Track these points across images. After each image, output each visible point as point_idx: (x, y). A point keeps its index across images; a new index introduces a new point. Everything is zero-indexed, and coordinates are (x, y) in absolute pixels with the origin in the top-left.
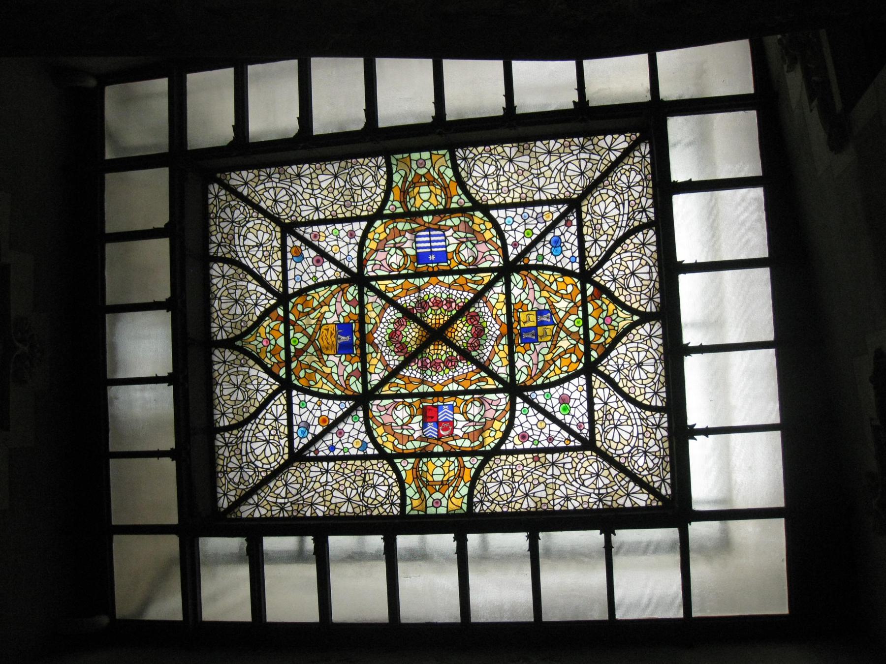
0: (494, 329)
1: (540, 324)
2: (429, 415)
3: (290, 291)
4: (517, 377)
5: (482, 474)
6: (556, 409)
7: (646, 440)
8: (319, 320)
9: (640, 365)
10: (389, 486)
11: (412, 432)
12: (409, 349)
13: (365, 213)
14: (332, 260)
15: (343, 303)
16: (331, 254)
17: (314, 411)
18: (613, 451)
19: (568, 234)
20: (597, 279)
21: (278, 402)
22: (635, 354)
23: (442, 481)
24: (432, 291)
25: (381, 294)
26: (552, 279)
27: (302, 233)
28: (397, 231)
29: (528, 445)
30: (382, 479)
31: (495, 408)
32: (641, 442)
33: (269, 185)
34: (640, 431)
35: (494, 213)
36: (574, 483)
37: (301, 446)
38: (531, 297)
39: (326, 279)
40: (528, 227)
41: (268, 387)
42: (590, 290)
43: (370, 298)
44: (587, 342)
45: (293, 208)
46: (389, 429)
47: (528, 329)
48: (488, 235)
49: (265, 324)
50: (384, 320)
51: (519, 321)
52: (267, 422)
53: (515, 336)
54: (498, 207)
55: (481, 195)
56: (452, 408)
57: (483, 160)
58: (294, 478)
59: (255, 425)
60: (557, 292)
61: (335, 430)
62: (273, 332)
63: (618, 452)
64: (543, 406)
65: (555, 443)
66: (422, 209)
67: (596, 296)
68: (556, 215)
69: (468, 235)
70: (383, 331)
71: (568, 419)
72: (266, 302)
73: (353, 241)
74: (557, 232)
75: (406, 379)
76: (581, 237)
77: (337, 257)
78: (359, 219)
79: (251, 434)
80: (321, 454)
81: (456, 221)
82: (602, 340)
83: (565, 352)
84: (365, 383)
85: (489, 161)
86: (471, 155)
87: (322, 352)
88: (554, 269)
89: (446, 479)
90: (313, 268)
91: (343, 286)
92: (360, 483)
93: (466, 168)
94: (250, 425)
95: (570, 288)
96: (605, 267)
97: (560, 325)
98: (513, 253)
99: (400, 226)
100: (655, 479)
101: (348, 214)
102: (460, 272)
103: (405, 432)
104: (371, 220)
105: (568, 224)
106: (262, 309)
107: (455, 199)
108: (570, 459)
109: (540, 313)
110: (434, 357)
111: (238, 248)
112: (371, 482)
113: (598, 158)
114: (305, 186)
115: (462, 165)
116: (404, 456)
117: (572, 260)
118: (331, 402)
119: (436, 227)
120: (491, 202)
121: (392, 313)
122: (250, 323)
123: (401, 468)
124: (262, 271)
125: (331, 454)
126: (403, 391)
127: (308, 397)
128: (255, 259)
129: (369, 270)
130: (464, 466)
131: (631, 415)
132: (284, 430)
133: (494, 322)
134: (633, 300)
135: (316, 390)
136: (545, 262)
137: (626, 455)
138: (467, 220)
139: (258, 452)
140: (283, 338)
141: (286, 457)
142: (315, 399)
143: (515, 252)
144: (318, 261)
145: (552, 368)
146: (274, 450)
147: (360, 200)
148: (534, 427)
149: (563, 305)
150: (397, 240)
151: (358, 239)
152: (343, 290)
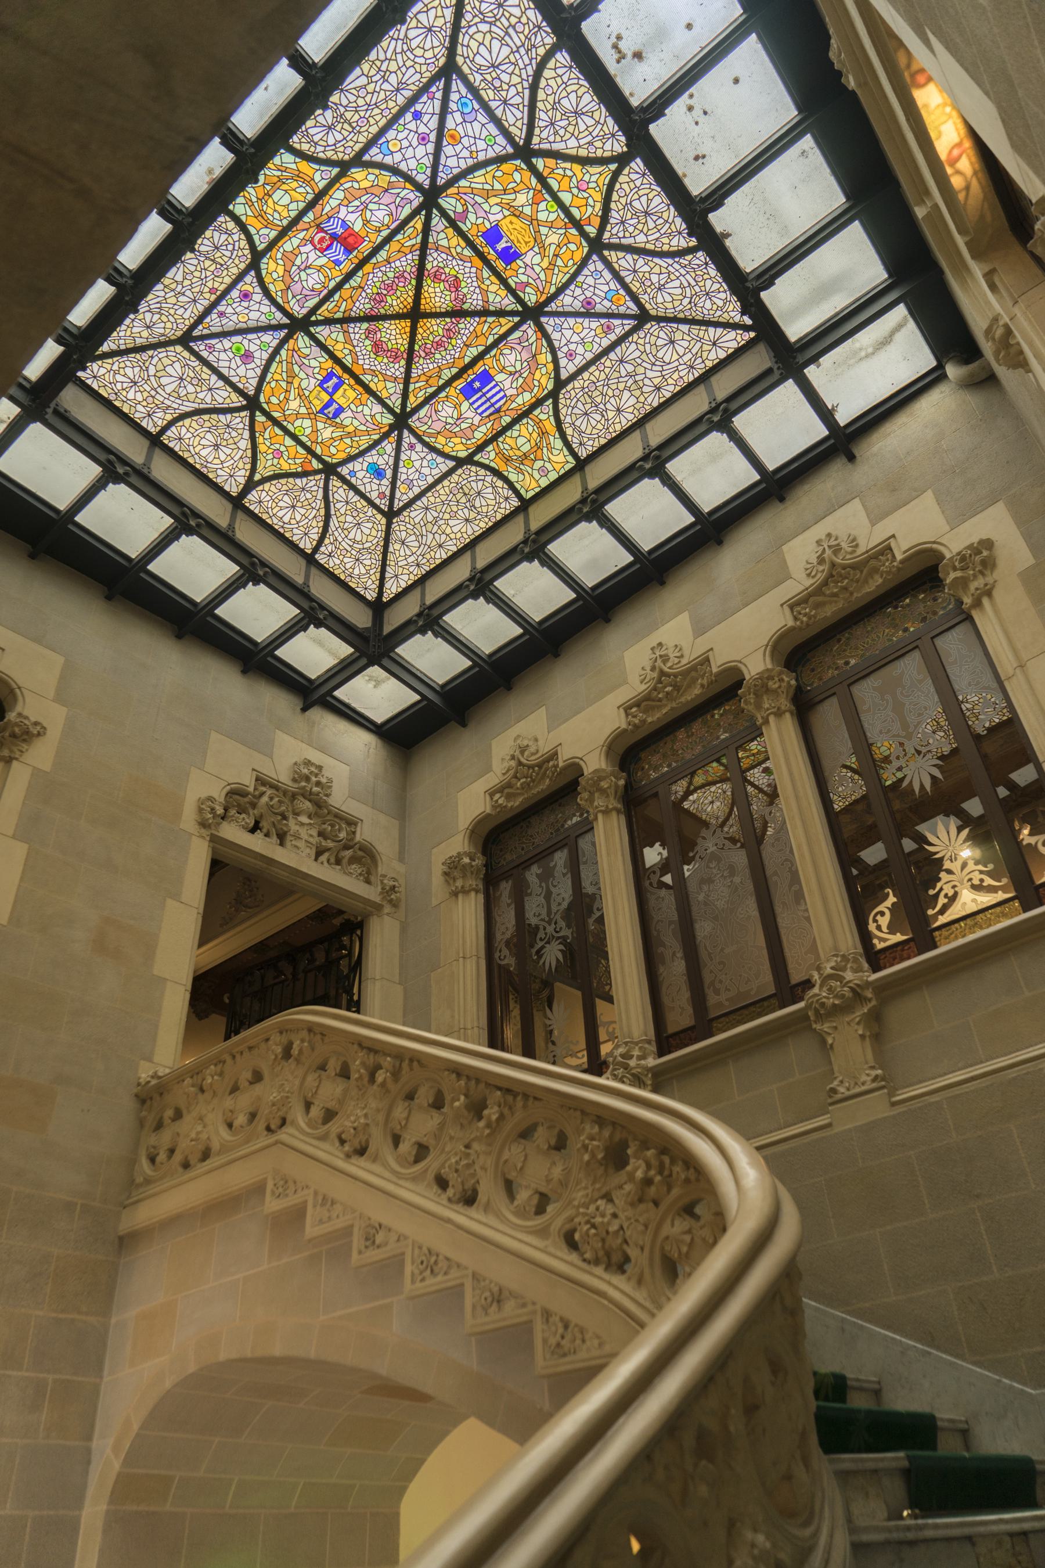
0: (367, 361)
2: (348, 240)
3: (595, 257)
4: (306, 338)
5: (243, 236)
6: (245, 342)
7: (145, 394)
8: (543, 248)
9: (216, 446)
10: (316, 144)
11: (350, 209)
12: (429, 282)
13: (569, 387)
14: (576, 314)
15: (531, 281)
16: (580, 320)
17: (472, 141)
18: (160, 356)
19: (375, 489)
20: (318, 477)
21: (519, 124)
22: (228, 451)
23: (270, 196)
24: (452, 352)
25: (501, 313)
26: (355, 444)
27: (625, 322)
28: (527, 388)
29: (235, 294)
30: (331, 141)
31: (298, 297)
32: (148, 389)
33: (686, 358)
34: (158, 397)
35: (451, 464)
36: (158, 305)
37: (454, 88)
38: (359, 416)
39: (568, 292)
40: (414, 469)
41: (544, 135)
42: (316, 465)
43: (508, 303)
45: (648, 346)
46: (375, 190)
47: (336, 387)
48: (441, 440)
49: (598, 206)
50: (477, 291)
51: (352, 387)
52: (513, 91)
54: (450, 472)
55: (472, 474)
56: (338, 263)
57: (491, 508)
58: (428, 46)
59: (524, 76)
60: (505, 190)
61: (433, 137)
62: (584, 202)
63: (156, 359)
64: (260, 335)
65: (214, 316)
66: (517, 427)
68: (398, 495)
69: (458, 429)
70: (469, 280)
71: (227, 343)
72: (614, 231)
73: (565, 349)
74: (385, 482)
75: (407, 251)
76: (362, 496)
77: (571, 321)
78: (573, 377)
79: (520, 62)
80: (424, 98)
81: (478, 435)
82: (267, 436)
83: (287, 399)
85: (485, 509)
86: (503, 506)
87: (514, 215)
88: (362, 453)
89: (270, 202)
90: (588, 294)
91: (544, 297)
92: (348, 115)
93: (500, 490)
94: (531, 73)
95: (333, 450)
96: (321, 491)
97: (312, 416)
98: (408, 438)
99: (527, 396)
100: (102, 371)
101: (586, 375)
102: (441, 389)
103: (357, 203)
104: (560, 384)
105: (381, 495)
106: (612, 221)
107: (492, 455)
108: (186, 316)
109: (340, 410)
110: (399, 294)
111: (683, 272)
112: (338, 128)
113: (400, 564)
114: (647, 382)
115: (505, 491)
116: (480, 448)
117: (352, 473)
118: (463, 166)
119: (492, 418)
120: (460, 471)
121: (475, 303)
122: (615, 197)
123: (487, 462)
124: (641, 262)
125: (412, 110)
126: (399, 237)
127: (491, 154)
128: (657, 270)
130: (266, 227)
131: (180, 402)
132: (488, 95)
133: (373, 368)
134: (273, 488)
135: (489, 169)
136: (374, 452)
137: (147, 364)
138: (469, 442)
139: (496, 44)
140: (568, 204)
141: (460, 60)
142: (482, 157)
143: (407, 440)
144: (589, 303)
145: (284, 374)
146: (478, 59)
147: (582, 399)
148: (247, 311)
149: (327, 434)
150: (521, 380)
151: (560, 354)
152: (542, 293)
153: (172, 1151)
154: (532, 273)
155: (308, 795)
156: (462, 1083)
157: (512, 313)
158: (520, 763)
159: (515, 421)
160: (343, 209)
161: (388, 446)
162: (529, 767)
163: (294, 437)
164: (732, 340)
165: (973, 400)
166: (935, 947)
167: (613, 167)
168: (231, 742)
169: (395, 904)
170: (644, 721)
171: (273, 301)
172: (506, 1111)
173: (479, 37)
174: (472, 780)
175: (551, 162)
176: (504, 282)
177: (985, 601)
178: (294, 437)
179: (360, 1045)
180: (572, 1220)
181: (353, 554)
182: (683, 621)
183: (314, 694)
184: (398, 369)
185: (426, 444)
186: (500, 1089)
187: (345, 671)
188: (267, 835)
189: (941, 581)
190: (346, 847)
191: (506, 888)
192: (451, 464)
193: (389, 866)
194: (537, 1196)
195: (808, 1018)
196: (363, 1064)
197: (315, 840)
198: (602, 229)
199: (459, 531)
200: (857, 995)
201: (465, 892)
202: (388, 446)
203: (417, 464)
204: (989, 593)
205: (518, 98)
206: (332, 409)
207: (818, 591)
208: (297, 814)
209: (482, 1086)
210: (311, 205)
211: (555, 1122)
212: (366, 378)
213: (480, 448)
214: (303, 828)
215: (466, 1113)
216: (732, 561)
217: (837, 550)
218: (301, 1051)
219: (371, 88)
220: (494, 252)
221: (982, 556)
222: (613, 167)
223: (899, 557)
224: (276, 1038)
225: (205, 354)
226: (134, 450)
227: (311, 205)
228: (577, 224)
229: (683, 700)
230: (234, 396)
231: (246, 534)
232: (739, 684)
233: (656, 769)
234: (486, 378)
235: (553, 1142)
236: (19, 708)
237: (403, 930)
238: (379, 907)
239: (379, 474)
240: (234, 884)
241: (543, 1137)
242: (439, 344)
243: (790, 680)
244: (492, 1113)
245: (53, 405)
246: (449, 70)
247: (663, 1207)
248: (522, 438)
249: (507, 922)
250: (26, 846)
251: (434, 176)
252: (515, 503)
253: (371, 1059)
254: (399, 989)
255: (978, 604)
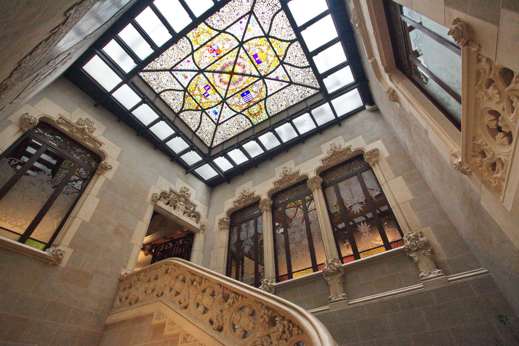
1: (206, 93)
2: (217, 51)
9: (174, 99)
14: (274, 79)
19: (214, 117)
25: (254, 76)
29: (186, 60)
35: (236, 113)
42: (200, 108)
43: (257, 74)
44: (191, 96)
47: (208, 89)
52: (267, 20)
53: (210, 86)
56: (214, 57)
67: (197, 107)
68: (220, 119)
78: (271, 95)
84: (244, 48)
88: (212, 107)
92: (223, 19)
97: (201, 95)
98: (225, 105)
102: (236, 93)
105: (216, 119)
109: (208, 95)
116: (244, 110)
117: (209, 112)
129: (261, 81)
141: (254, 10)
153: (127, 298)
154: (263, 68)
155: (183, 196)
156: (222, 289)
157: (257, 77)
158: (243, 195)
159: (254, 104)
160: (218, 43)
161: (220, 107)
162: (246, 196)
163: (195, 100)
164: (313, 92)
165: (372, 115)
166: (360, 258)
167: (289, 43)
168: (163, 179)
169: (204, 230)
170: (279, 187)
171: (196, 64)
172: (235, 300)
173: (260, 5)
174: (229, 199)
175: (273, 40)
176: (256, 68)
177: (376, 164)
178: (195, 100)
179: (190, 272)
180: (256, 342)
181: (206, 131)
182: (292, 162)
183: (190, 170)
184: (226, 87)
185: (230, 107)
186: (234, 292)
187: (199, 164)
188: (171, 206)
189: (363, 158)
190: (192, 213)
191: (235, 229)
192: (236, 113)
193: (203, 219)
194: (244, 332)
195: (323, 275)
196: (190, 278)
197: (184, 209)
198: (284, 59)
199: (235, 131)
200: (338, 270)
201: (224, 229)
202: (220, 107)
203: (226, 112)
204: (377, 162)
205: (268, 22)
206: (206, 95)
207: (330, 157)
208: (180, 201)
209: (228, 291)
210: (210, 40)
211: (254, 308)
212: (216, 88)
213: (244, 110)
214: (181, 205)
215: (222, 299)
216: (305, 148)
217: (336, 148)
218: (171, 272)
219: (230, 13)
220: (256, 60)
221: (375, 153)
222: (289, 43)
223: (352, 151)
224: (164, 266)
225: (175, 75)
226: (152, 97)
227: (210, 40)
228: (278, 56)
229: (291, 182)
230: (181, 87)
231: (177, 123)
232: (307, 179)
233: (281, 200)
234: (248, 92)
235: (251, 313)
236: (105, 161)
237: (205, 238)
238: (199, 231)
239: (216, 113)
240: (159, 220)
241: (247, 310)
242: (237, 82)
243: (321, 180)
244: (230, 301)
245: (131, 80)
246: (251, 12)
247: (289, 342)
248: (255, 109)
249: (235, 238)
250: (99, 200)
251: (243, 39)
252: (251, 125)
253: (193, 278)
254: (202, 254)
255: (374, 165)
